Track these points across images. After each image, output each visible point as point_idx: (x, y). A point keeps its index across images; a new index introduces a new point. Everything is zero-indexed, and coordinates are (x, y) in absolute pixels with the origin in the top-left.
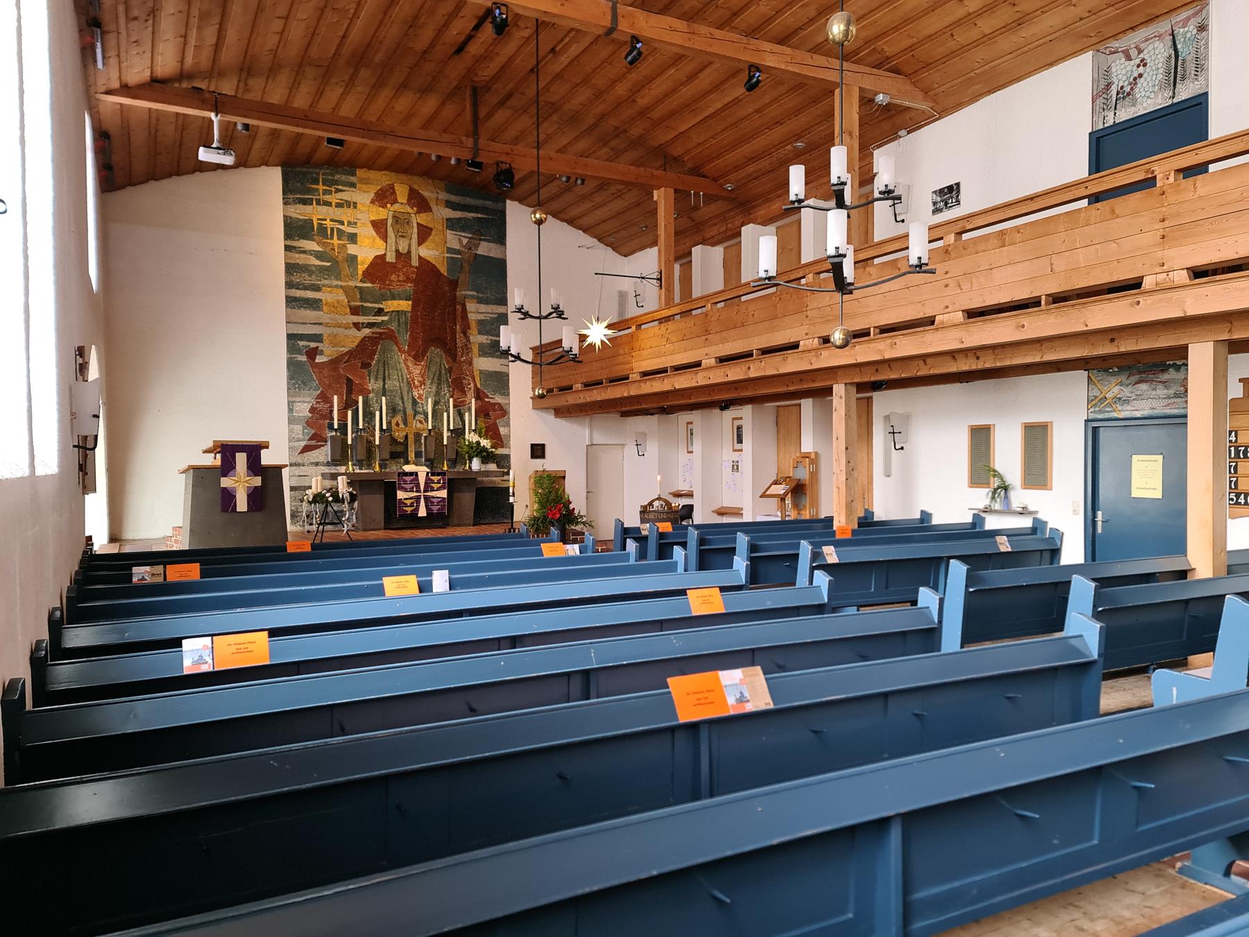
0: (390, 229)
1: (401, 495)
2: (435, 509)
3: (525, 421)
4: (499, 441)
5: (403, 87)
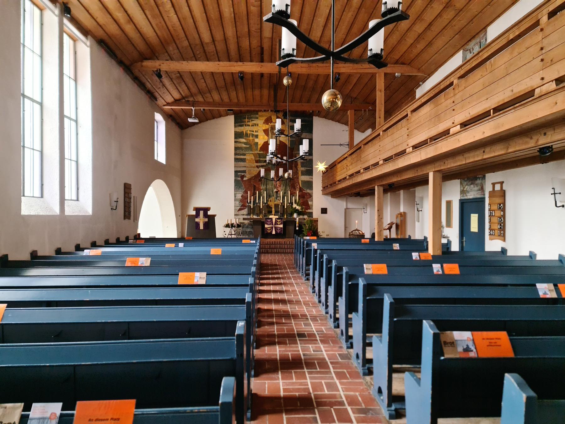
0: (270, 132)
1: (266, 226)
2: (278, 231)
3: (319, 199)
4: (309, 207)
5: (253, 88)
